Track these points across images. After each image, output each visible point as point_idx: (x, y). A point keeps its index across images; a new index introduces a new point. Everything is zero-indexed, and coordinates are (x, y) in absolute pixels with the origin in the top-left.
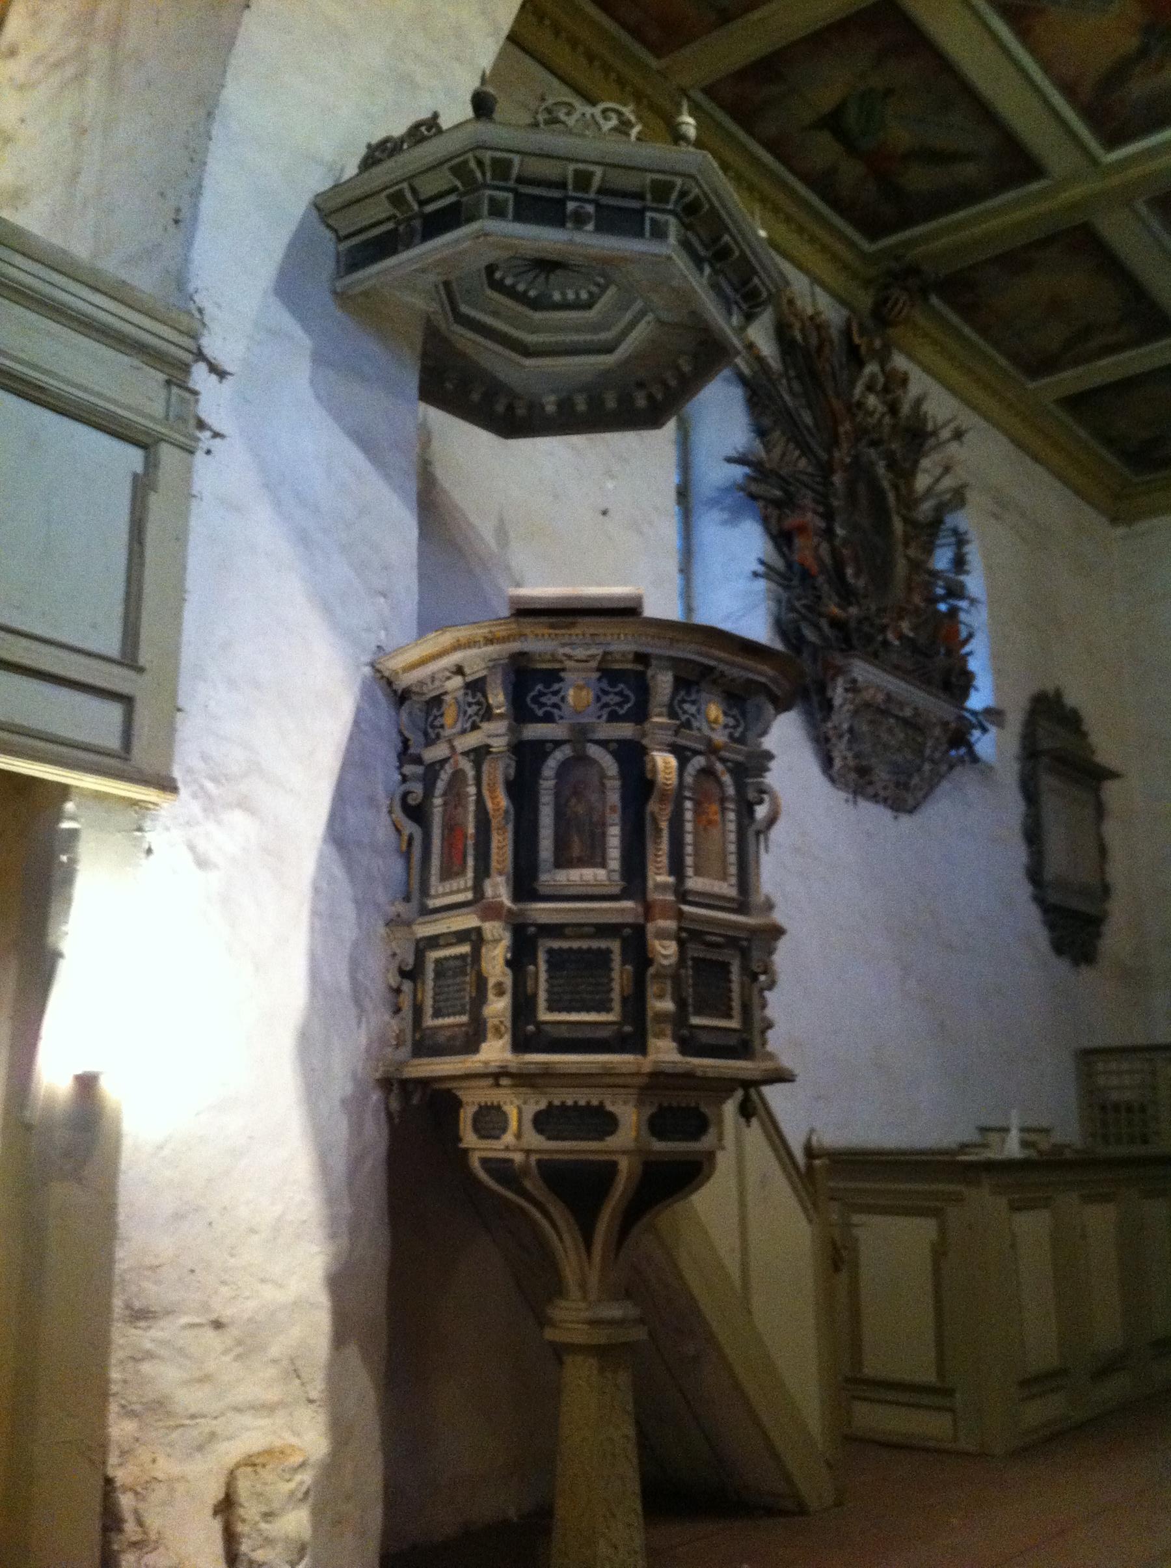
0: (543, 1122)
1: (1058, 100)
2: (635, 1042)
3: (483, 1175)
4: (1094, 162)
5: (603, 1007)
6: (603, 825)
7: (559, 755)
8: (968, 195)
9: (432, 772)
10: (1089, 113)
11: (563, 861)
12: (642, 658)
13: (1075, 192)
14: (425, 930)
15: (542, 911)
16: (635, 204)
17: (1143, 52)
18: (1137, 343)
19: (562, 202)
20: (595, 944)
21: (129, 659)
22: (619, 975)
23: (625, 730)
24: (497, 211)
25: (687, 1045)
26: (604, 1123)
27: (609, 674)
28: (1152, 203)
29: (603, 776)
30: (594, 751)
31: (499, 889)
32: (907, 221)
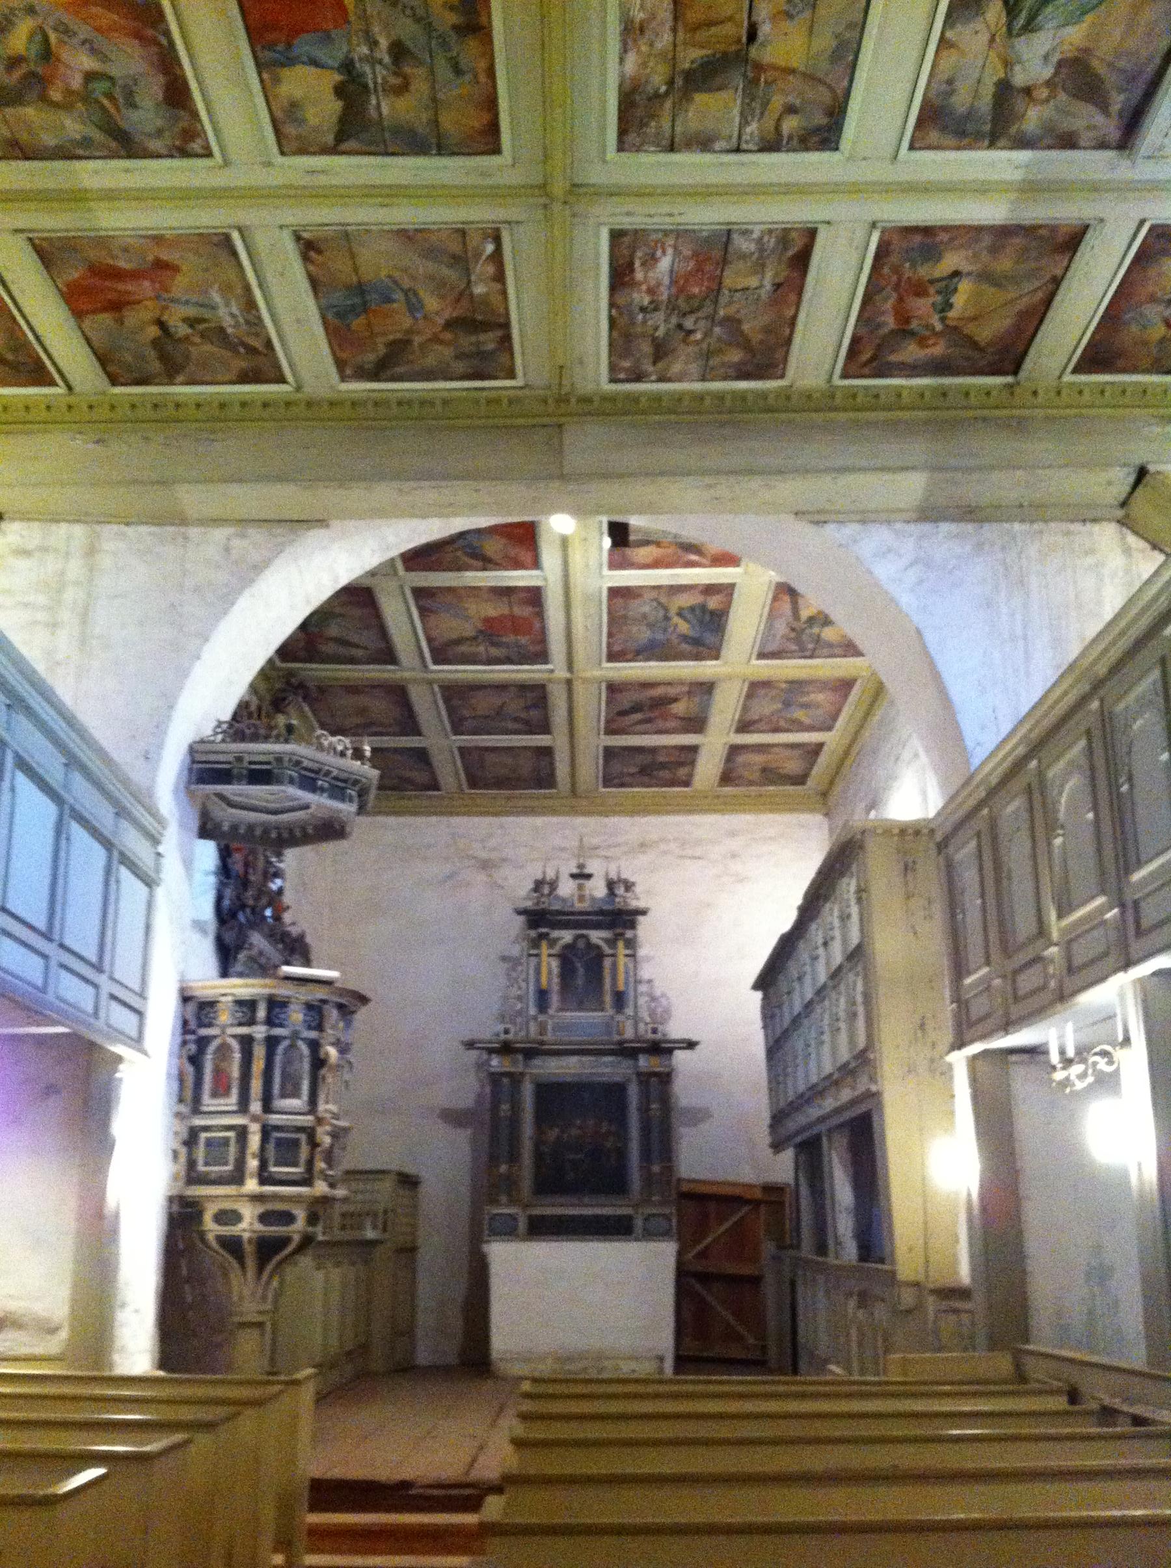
0: (264, 1218)
1: (424, 644)
2: (307, 1181)
3: (214, 1244)
4: (426, 666)
5: (295, 1165)
6: (301, 1078)
7: (286, 1043)
8: (352, 661)
9: (203, 1042)
10: (433, 650)
11: (283, 1096)
12: (324, 1002)
13: (407, 675)
14: (199, 1122)
15: (275, 1119)
16: (343, 785)
17: (475, 638)
18: (395, 734)
19: (314, 780)
20: (293, 1136)
21: (142, 995)
22: (304, 1152)
23: (313, 1034)
24: (291, 781)
25: (263, 1181)
26: (288, 1218)
27: (309, 1007)
28: (440, 687)
29: (301, 1056)
30: (300, 1044)
31: (256, 1107)
32: (310, 660)
